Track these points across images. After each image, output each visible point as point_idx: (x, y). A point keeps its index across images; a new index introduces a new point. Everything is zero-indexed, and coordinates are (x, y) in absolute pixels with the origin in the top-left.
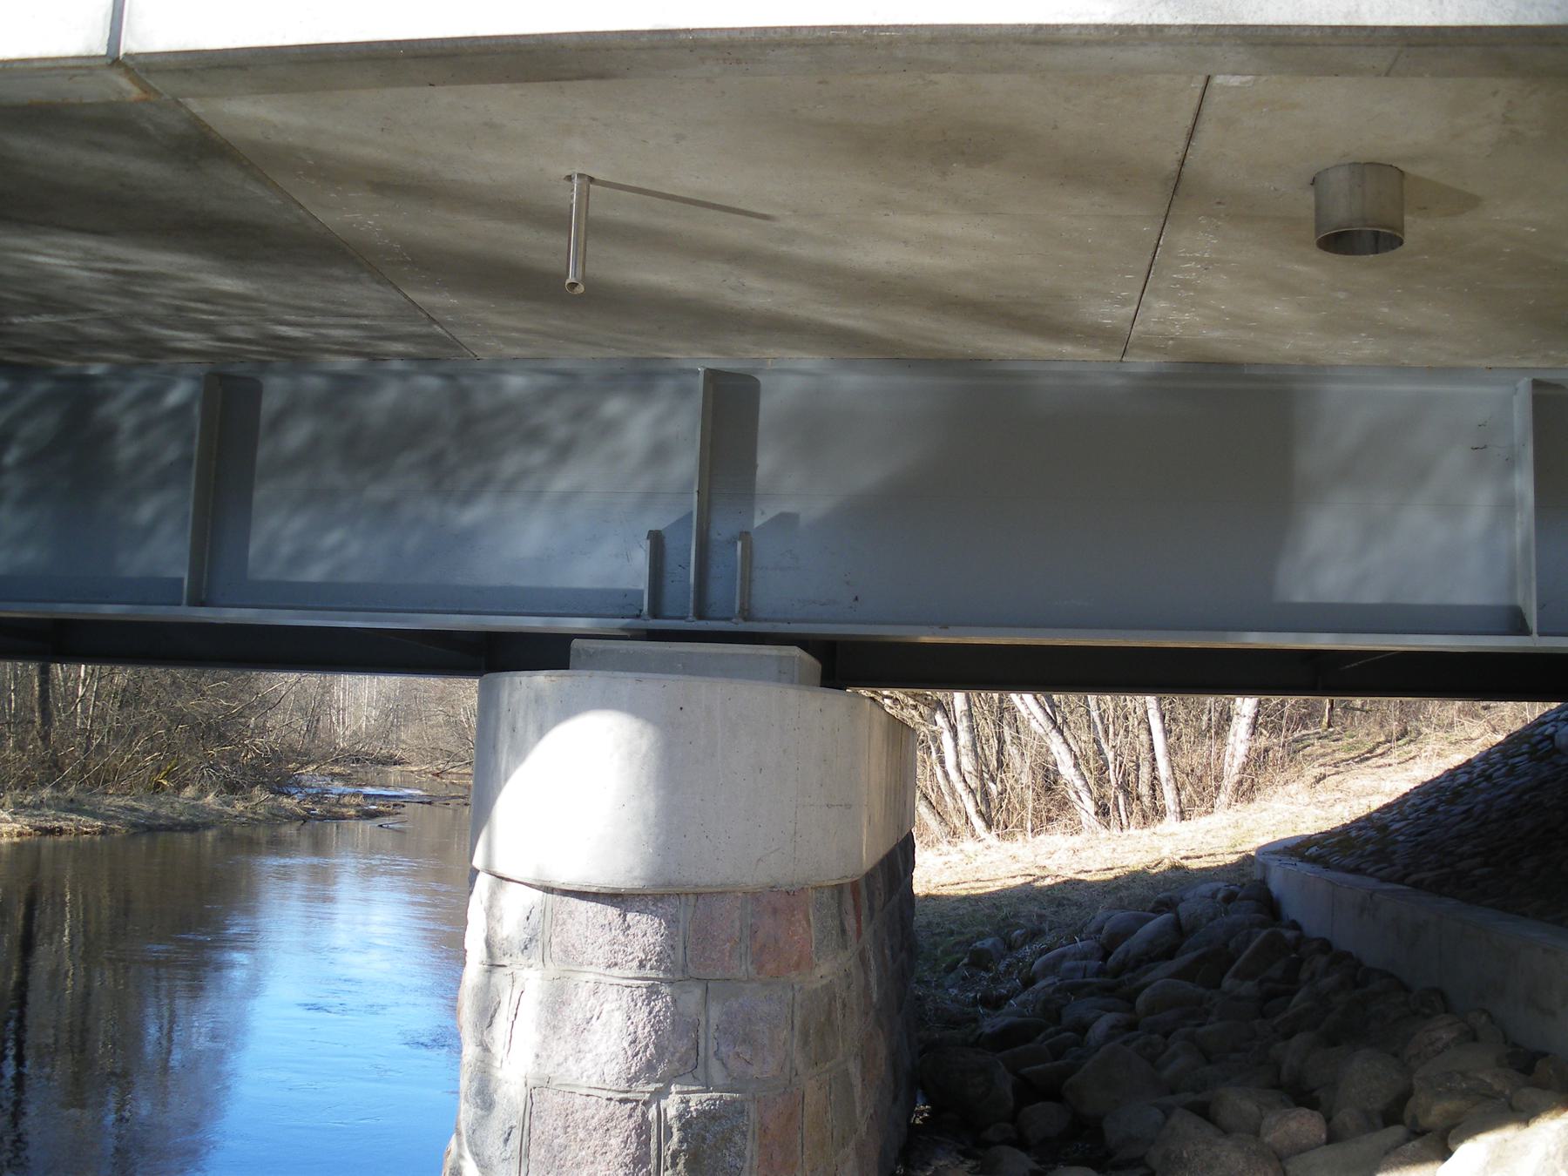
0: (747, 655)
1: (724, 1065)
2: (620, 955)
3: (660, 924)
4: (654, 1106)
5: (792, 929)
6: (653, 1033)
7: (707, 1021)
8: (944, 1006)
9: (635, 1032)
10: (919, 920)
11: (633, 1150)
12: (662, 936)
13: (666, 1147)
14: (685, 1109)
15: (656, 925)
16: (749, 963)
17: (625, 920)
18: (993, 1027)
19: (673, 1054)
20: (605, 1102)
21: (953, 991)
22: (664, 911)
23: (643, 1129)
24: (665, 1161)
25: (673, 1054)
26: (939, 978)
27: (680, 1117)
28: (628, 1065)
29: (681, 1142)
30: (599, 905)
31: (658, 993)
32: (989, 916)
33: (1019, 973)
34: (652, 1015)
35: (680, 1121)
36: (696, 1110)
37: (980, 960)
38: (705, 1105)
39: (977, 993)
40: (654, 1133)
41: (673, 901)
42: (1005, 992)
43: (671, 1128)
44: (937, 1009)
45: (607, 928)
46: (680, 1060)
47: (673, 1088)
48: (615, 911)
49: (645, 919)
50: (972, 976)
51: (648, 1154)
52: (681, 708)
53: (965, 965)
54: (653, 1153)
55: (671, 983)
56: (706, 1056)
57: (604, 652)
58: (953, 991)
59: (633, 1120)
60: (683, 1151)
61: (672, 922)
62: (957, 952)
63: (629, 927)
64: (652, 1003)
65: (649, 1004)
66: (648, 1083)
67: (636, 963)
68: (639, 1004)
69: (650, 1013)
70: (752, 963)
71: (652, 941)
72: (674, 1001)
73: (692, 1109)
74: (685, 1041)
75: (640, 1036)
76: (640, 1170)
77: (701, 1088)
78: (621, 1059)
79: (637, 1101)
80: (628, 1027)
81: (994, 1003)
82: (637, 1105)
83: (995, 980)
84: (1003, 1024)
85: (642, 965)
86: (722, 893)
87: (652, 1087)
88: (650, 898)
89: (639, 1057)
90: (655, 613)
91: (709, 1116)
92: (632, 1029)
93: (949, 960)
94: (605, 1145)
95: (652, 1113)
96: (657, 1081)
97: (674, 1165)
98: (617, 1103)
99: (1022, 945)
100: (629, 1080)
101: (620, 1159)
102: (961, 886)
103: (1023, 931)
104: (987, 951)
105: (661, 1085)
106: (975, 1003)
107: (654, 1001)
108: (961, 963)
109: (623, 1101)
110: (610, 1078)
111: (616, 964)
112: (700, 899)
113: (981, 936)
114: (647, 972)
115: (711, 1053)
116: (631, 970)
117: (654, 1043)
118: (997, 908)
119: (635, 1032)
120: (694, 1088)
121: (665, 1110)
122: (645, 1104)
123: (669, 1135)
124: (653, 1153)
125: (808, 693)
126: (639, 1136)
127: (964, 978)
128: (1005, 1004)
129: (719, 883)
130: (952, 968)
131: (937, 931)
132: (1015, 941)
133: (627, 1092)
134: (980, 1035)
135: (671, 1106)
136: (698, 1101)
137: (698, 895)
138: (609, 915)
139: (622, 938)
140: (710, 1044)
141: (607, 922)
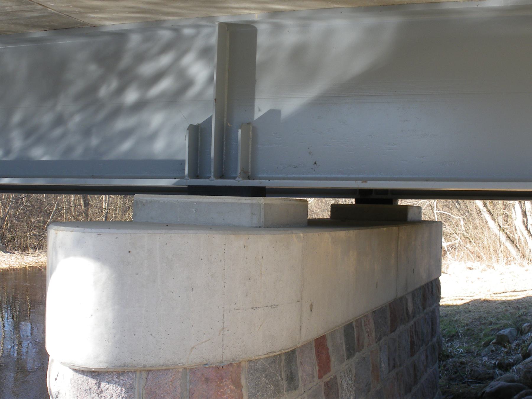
0: (232, 204)
3: (122, 390)
5: (221, 390)
8: (477, 368)
10: (440, 327)
15: (119, 391)
17: (99, 387)
18: (491, 388)
21: (485, 359)
22: (124, 382)
26: (479, 350)
30: (85, 377)
32: (512, 314)
33: (522, 350)
37: (502, 341)
39: (496, 361)
41: (131, 375)
42: (512, 361)
44: (472, 370)
45: (88, 392)
48: (93, 382)
49: (111, 387)
50: (497, 350)
52: (129, 252)
53: (494, 343)
57: (151, 202)
58: (485, 359)
62: (492, 335)
63: (102, 391)
81: (505, 367)
83: (508, 353)
84: (497, 386)
86: (165, 370)
88: (115, 373)
90: (195, 174)
93: (486, 339)
99: (527, 333)
102: (506, 294)
103: (529, 324)
104: (506, 336)
106: (495, 366)
108: (491, 343)
112: (150, 373)
113: (505, 327)
125: (232, 237)
127: (492, 351)
128: (510, 368)
129: (162, 364)
130: (487, 344)
131: (483, 322)
132: (524, 330)
134: (484, 392)
137: (149, 371)
138: (90, 383)
141: (88, 388)
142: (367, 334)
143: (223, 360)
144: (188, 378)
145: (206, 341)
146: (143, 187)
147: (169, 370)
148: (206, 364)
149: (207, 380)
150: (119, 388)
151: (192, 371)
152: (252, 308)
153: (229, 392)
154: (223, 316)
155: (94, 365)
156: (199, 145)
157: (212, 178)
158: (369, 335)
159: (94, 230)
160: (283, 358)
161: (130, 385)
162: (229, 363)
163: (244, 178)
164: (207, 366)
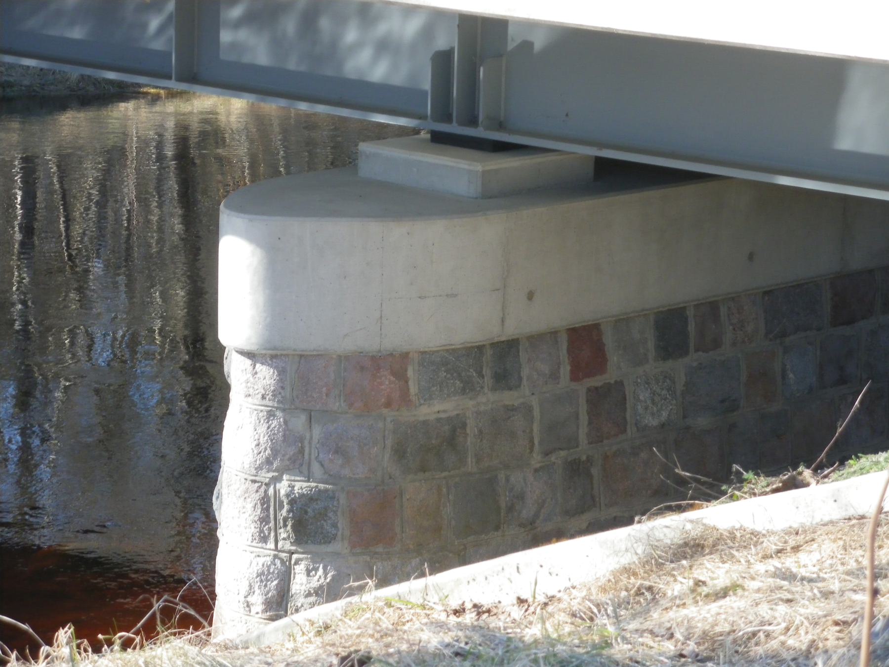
1: (322, 465)
2: (251, 390)
3: (274, 372)
4: (272, 487)
5: (378, 380)
6: (269, 441)
7: (311, 438)
9: (259, 439)
11: (259, 513)
12: (275, 380)
13: (280, 514)
14: (291, 491)
15: (271, 373)
16: (342, 401)
17: (254, 368)
19: (284, 456)
20: (243, 481)
23: (265, 501)
24: (279, 523)
25: (284, 456)
27: (287, 495)
28: (255, 459)
29: (289, 511)
31: (274, 416)
34: (269, 430)
35: (288, 498)
36: (298, 492)
38: (304, 490)
40: (272, 504)
43: (283, 502)
45: (244, 372)
46: (290, 459)
47: (285, 477)
51: (268, 516)
54: (272, 516)
55: (284, 410)
56: (310, 459)
59: (258, 494)
60: (290, 518)
61: (282, 372)
63: (256, 373)
64: (270, 422)
65: (268, 422)
66: (268, 472)
67: (260, 396)
68: (262, 422)
69: (268, 428)
70: (345, 401)
71: (268, 383)
72: (286, 422)
73: (296, 492)
74: (294, 448)
75: (261, 442)
76: (264, 526)
77: (303, 479)
78: (251, 456)
79: (262, 483)
80: (255, 436)
82: (262, 485)
85: (263, 397)
87: (270, 475)
89: (261, 455)
91: (309, 499)
92: (257, 437)
94: (244, 507)
95: (271, 491)
96: (274, 471)
97: (285, 526)
98: (250, 482)
100: (256, 469)
101: (252, 517)
105: (277, 474)
107: (272, 420)
109: (254, 481)
110: (247, 466)
111: (249, 395)
114: (267, 402)
115: (313, 457)
116: (257, 400)
117: (270, 447)
118: (214, 420)
119: (259, 439)
120: (299, 478)
121: (279, 490)
122: (266, 484)
123: (281, 506)
124: (272, 516)
126: (262, 505)
133: (256, 476)
135: (283, 487)
136: (301, 486)
137: (301, 356)
139: (251, 379)
140: (313, 451)
142: (731, 327)
143: (382, 349)
144: (343, 365)
145: (361, 329)
146: (717, 45)
147: (321, 355)
148: (362, 353)
149: (362, 368)
150: (272, 370)
151: (347, 358)
152: (420, 297)
153: (387, 383)
154: (381, 304)
155: (247, 347)
156: (503, 79)
157: (455, 124)
158: (734, 329)
159: (246, 216)
160: (489, 352)
161: (282, 368)
162: (388, 353)
163: (488, 128)
164: (362, 354)
